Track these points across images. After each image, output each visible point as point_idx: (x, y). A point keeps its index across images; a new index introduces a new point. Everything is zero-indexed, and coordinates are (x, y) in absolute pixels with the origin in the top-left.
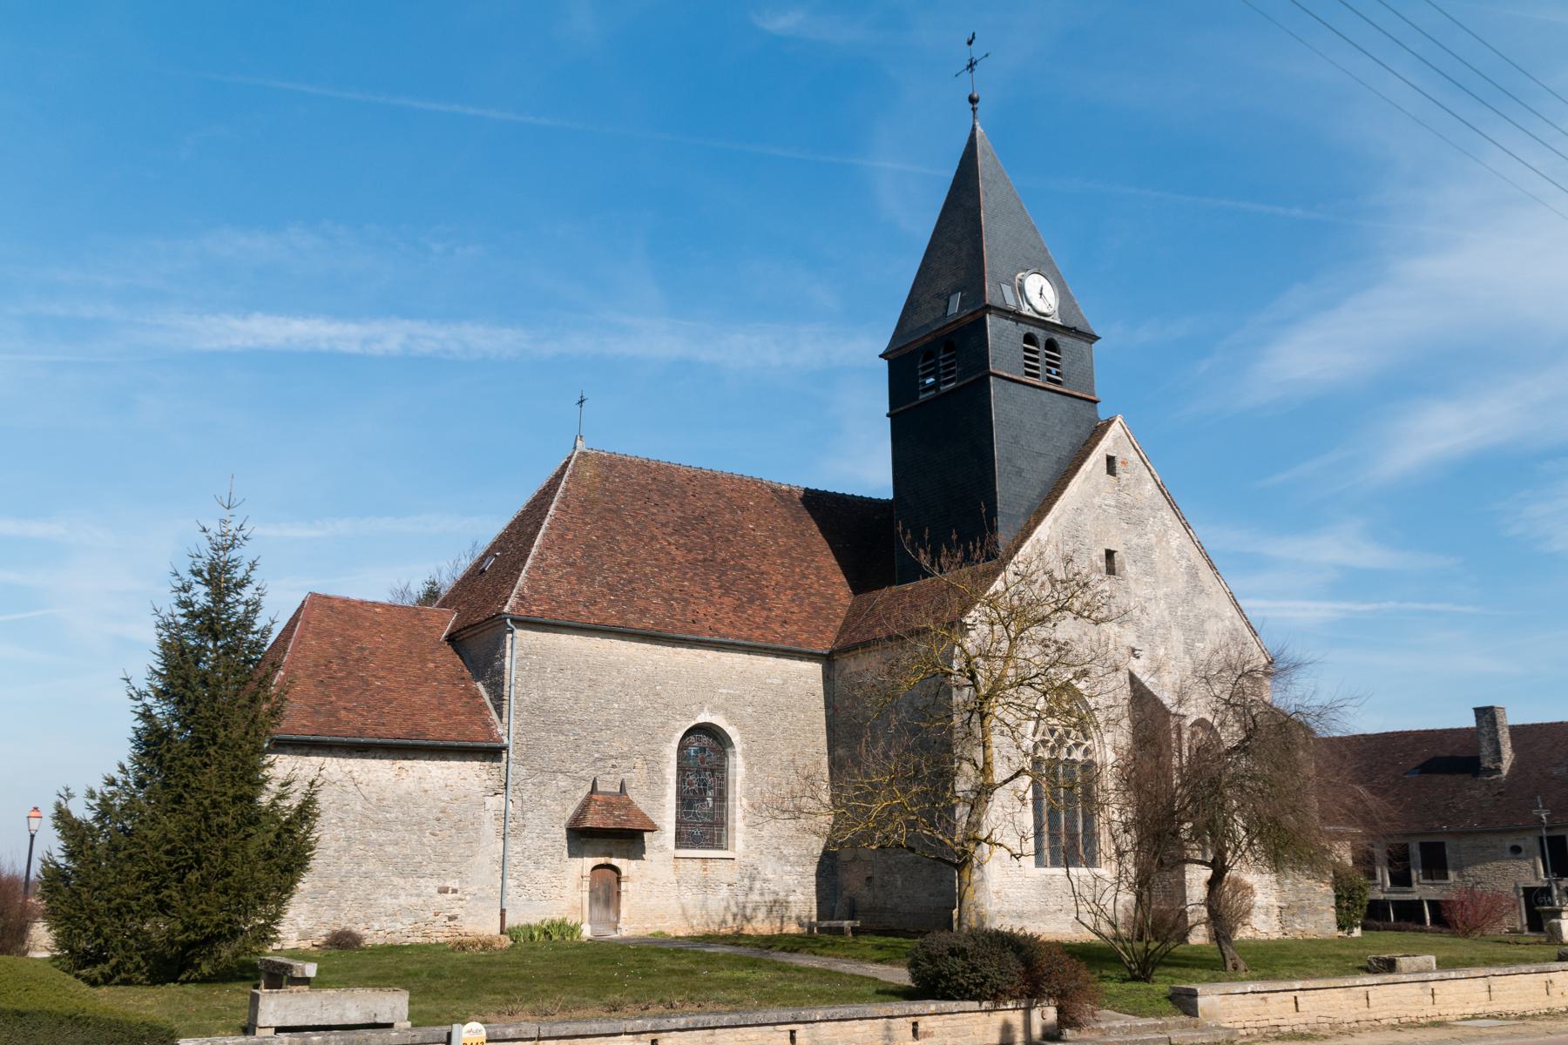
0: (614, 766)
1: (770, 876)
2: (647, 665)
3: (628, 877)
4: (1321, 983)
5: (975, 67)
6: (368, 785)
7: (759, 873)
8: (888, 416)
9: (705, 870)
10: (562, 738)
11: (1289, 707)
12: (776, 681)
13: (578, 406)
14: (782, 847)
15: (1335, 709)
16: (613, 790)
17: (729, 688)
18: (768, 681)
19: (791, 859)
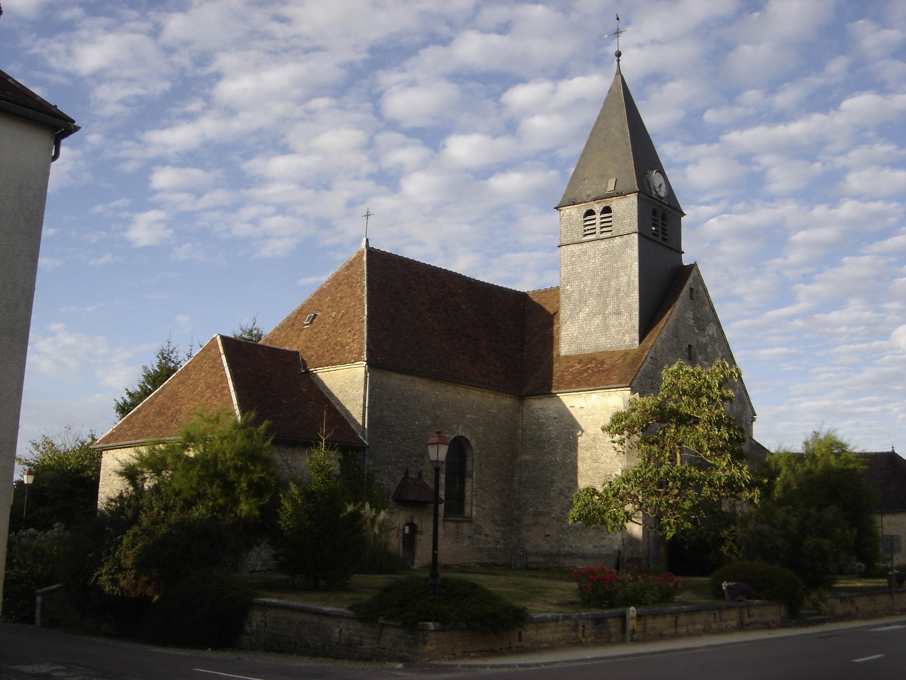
0: (415, 461)
1: (488, 533)
2: (433, 398)
3: (421, 531)
4: (576, 664)
5: (620, 34)
6: (295, 469)
7: (483, 531)
8: (56, 106)
9: (458, 528)
10: (391, 442)
11: (207, 455)
12: (494, 411)
13: (365, 218)
14: (495, 515)
15: (122, 463)
16: (415, 477)
17: (472, 414)
18: (491, 411)
19: (499, 522)
